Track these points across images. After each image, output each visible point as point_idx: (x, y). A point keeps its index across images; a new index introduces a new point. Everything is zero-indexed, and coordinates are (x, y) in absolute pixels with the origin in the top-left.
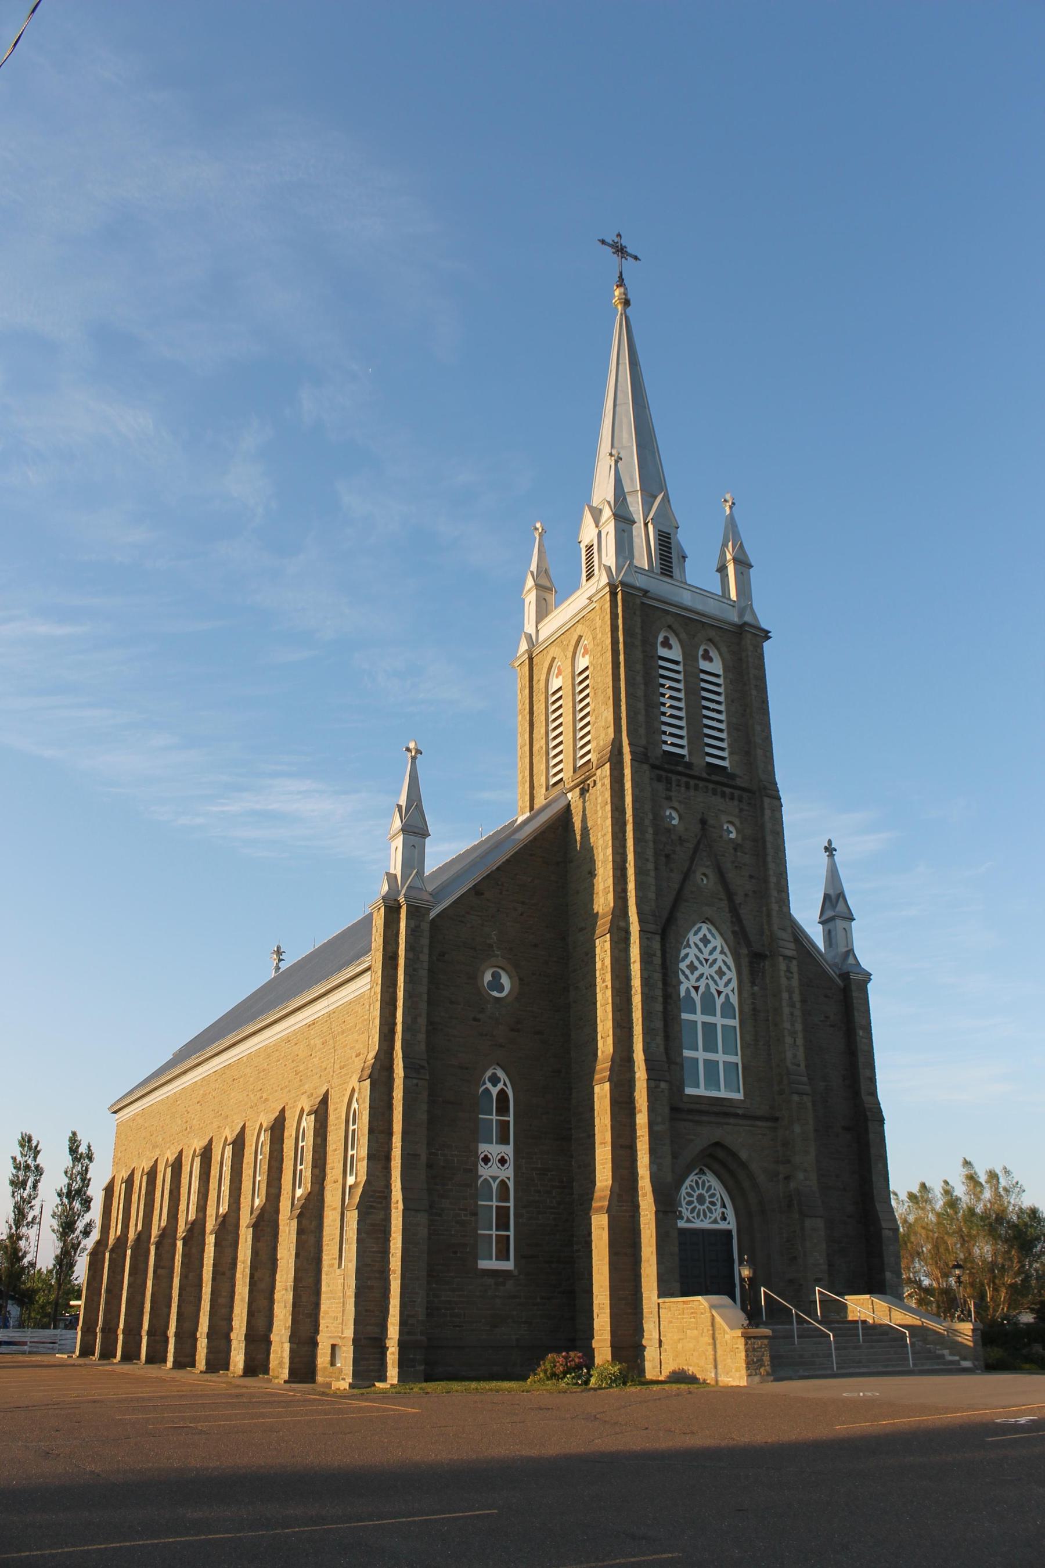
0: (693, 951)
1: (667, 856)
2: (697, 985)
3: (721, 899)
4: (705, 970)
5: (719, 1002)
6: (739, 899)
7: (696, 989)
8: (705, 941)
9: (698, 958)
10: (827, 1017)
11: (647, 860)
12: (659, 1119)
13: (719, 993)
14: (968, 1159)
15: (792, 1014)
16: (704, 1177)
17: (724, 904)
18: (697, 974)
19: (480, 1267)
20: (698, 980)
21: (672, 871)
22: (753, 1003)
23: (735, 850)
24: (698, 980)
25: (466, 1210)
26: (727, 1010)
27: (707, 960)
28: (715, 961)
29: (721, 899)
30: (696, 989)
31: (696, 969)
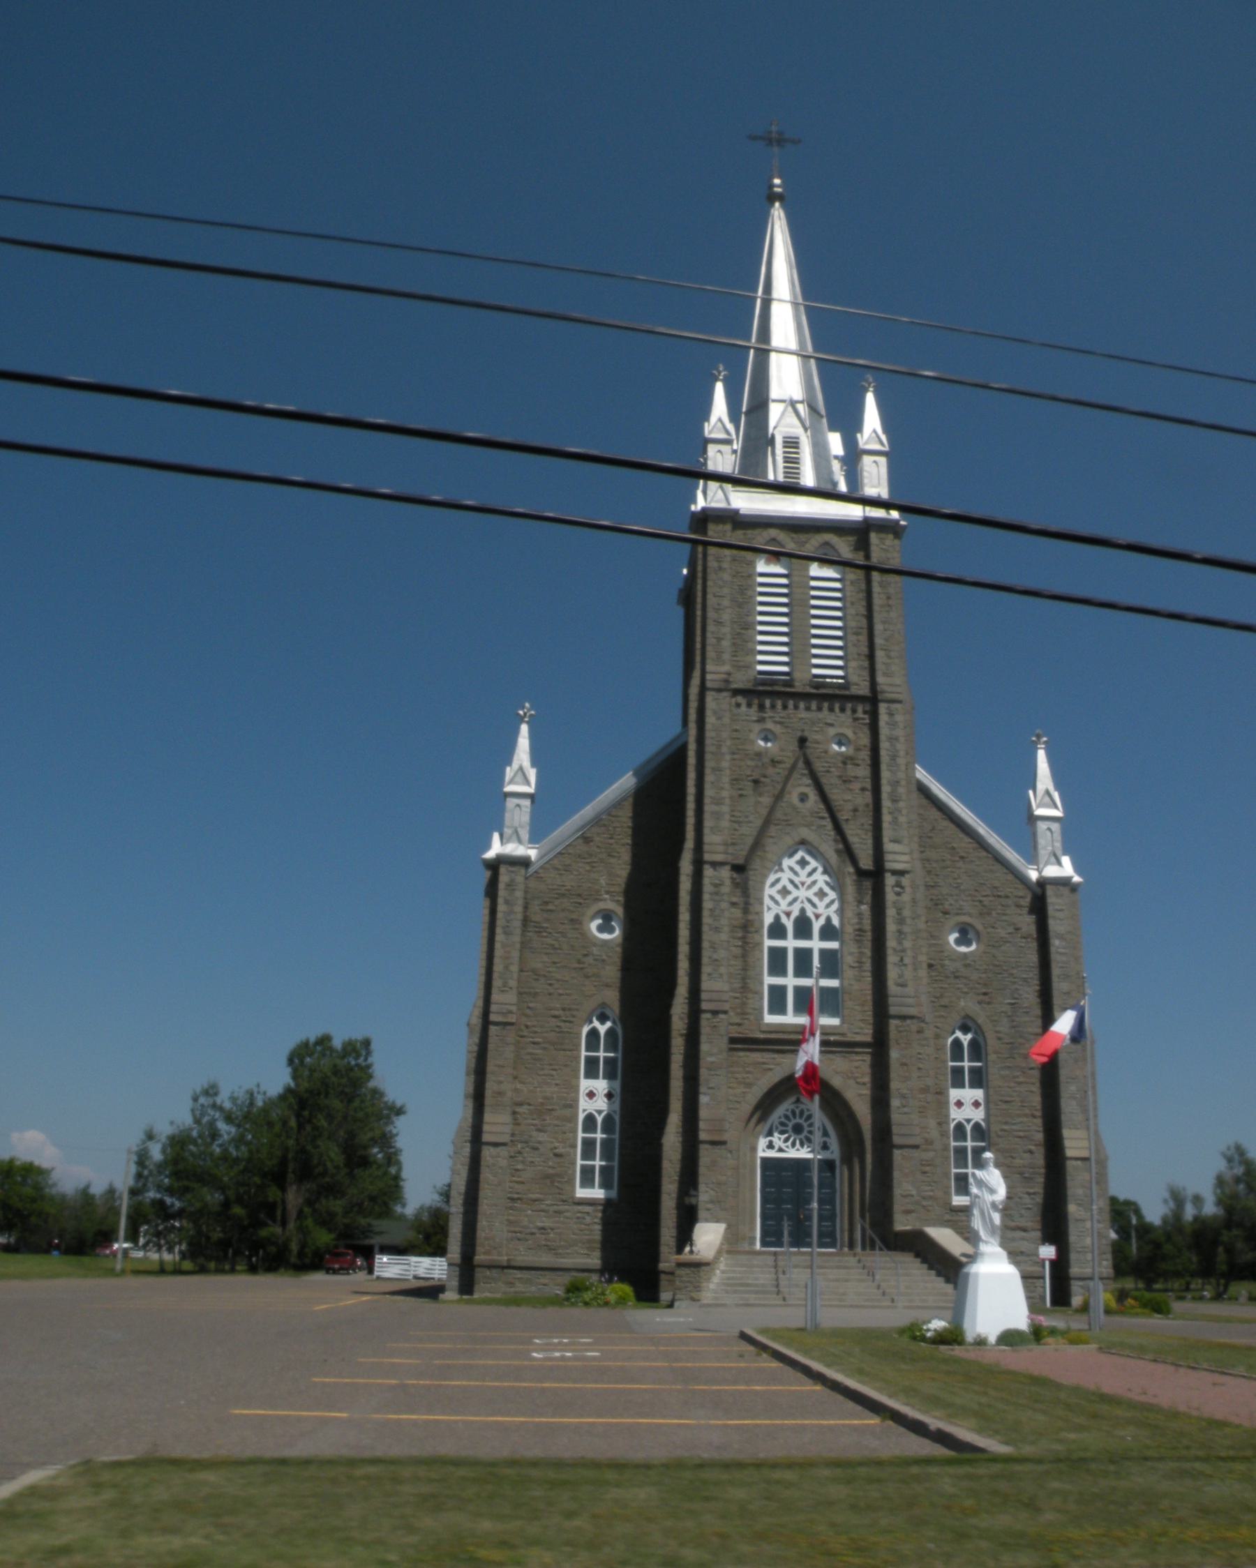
0: (785, 877)
1: (756, 782)
2: (788, 909)
3: (823, 818)
4: (802, 893)
5: (817, 926)
6: (842, 816)
7: (788, 914)
8: (803, 863)
9: (792, 882)
10: (1017, 929)
11: (722, 788)
12: (715, 1051)
13: (817, 916)
14: (373, 1046)
15: (900, 932)
16: (802, 1106)
17: (828, 823)
18: (790, 898)
19: (1018, 1317)
20: (791, 904)
21: (761, 795)
22: (859, 923)
23: (844, 763)
24: (791, 904)
25: (526, 1142)
26: (828, 932)
27: (803, 884)
28: (814, 883)
29: (823, 818)
30: (788, 914)
31: (789, 893)
